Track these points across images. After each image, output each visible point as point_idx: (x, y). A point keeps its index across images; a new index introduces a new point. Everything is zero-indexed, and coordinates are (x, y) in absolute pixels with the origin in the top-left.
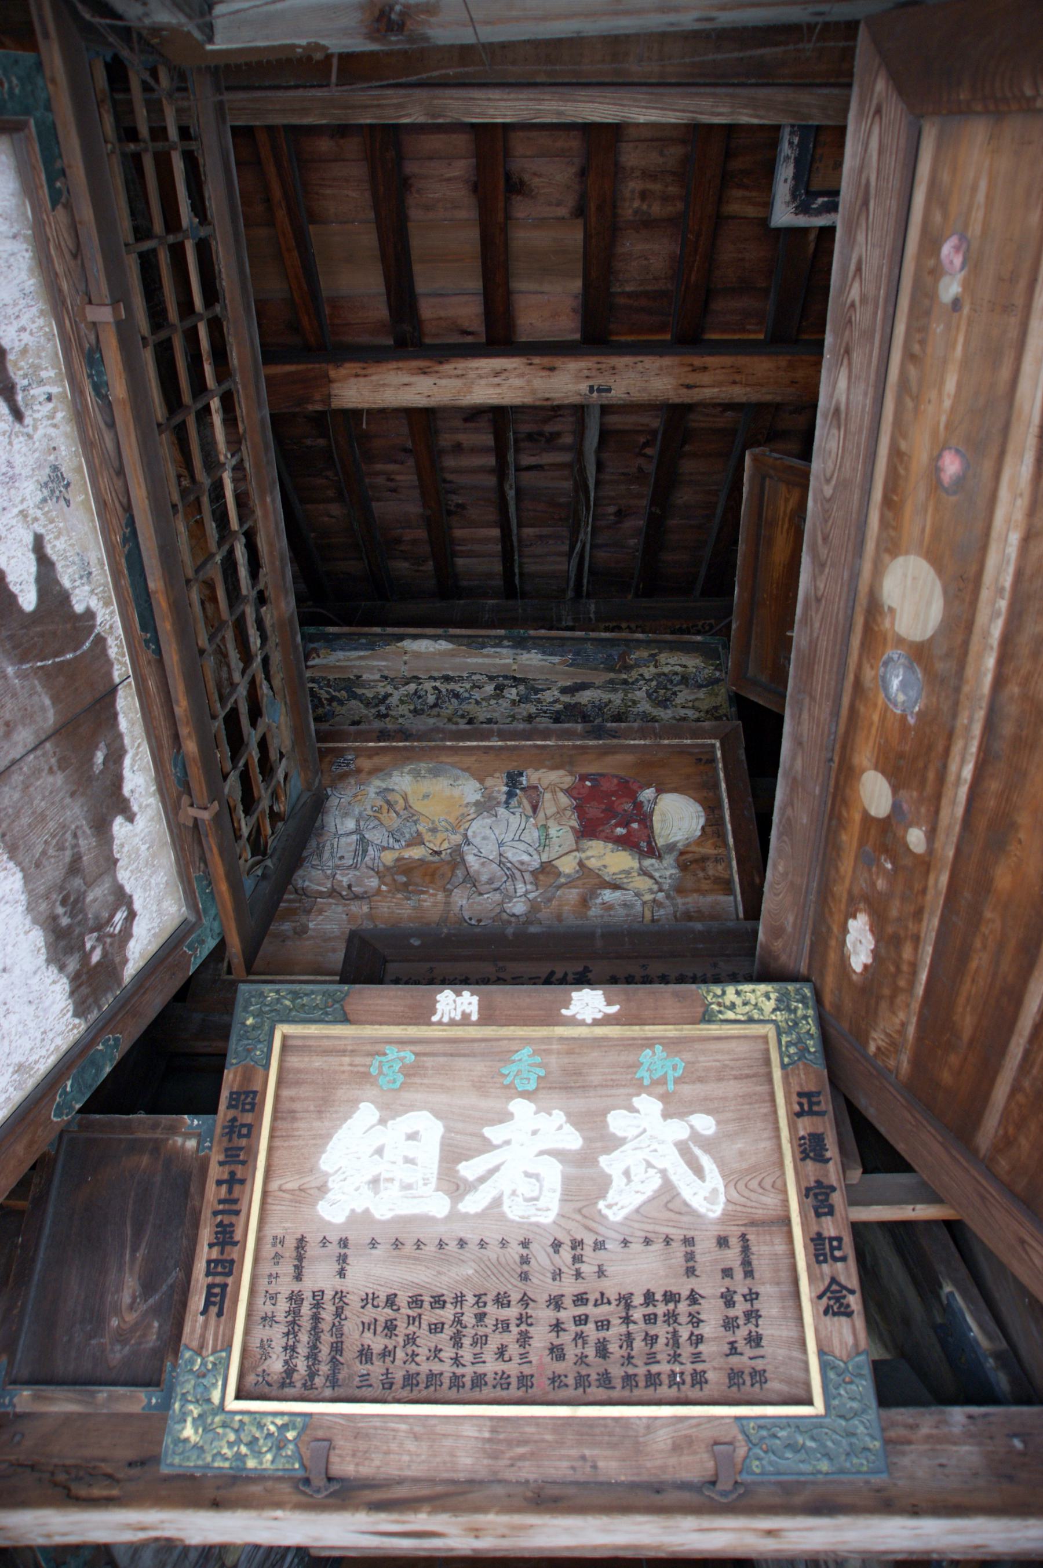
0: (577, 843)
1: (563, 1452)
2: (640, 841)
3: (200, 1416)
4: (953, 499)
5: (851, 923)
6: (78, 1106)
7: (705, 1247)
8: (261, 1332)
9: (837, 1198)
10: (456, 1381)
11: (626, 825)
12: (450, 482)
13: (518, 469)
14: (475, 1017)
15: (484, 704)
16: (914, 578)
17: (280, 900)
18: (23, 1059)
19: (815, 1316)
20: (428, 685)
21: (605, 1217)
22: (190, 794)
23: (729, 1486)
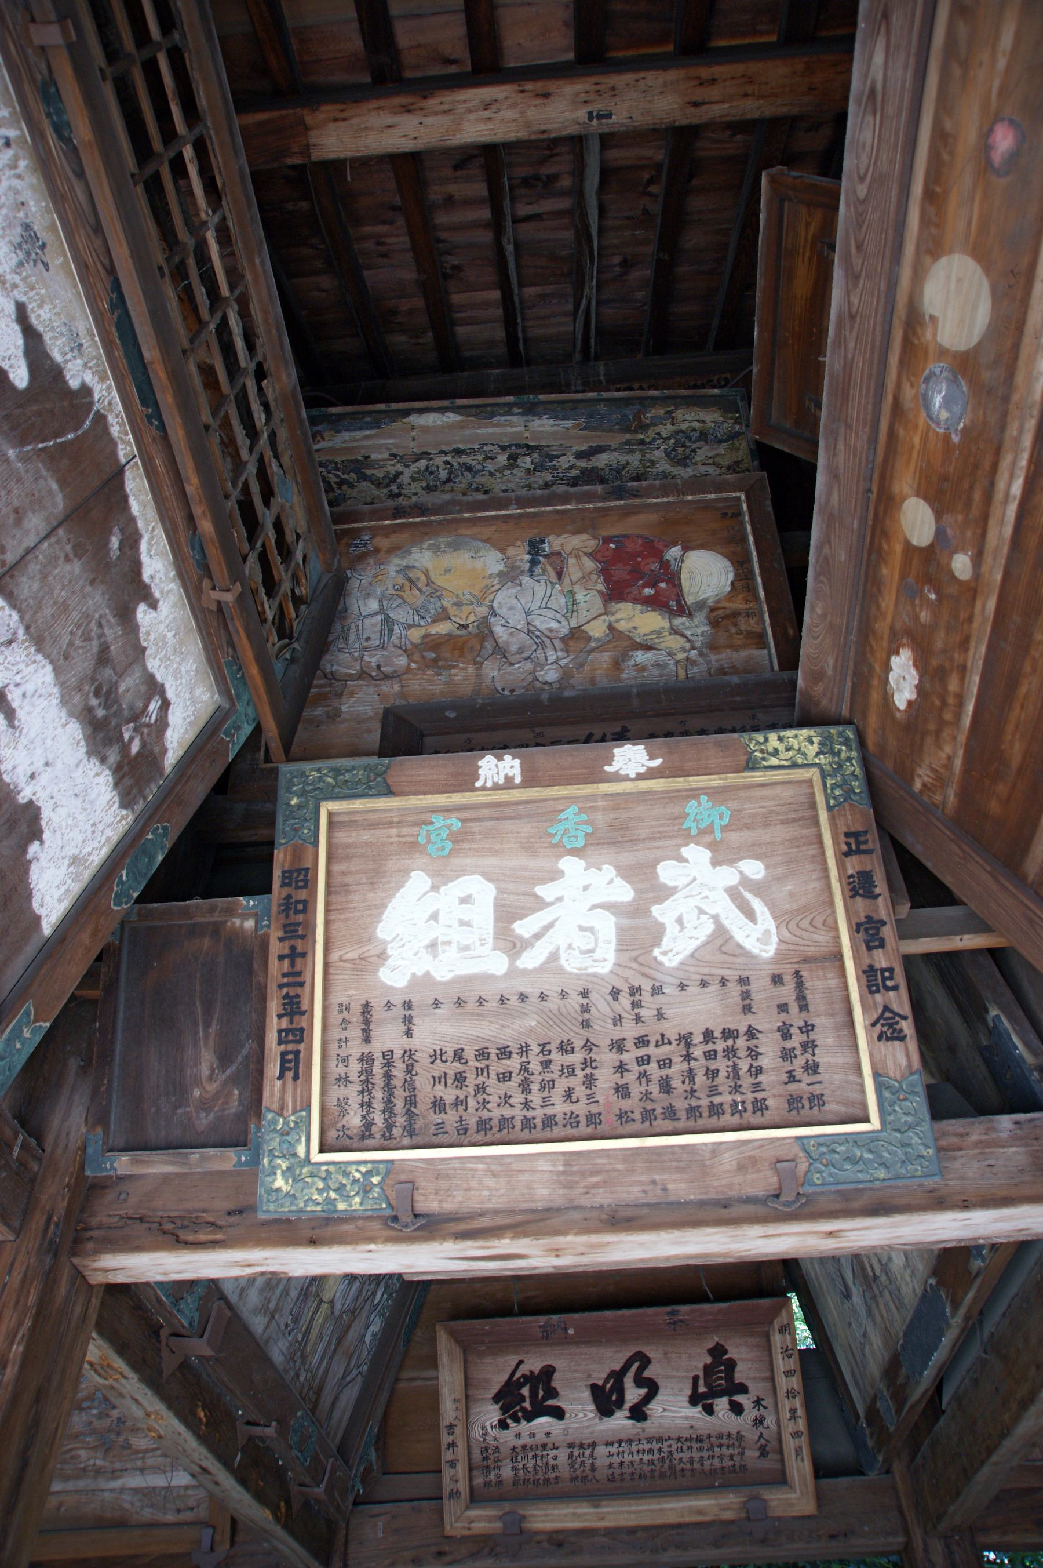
0: (605, 606)
1: (634, 1178)
2: (670, 601)
3: (288, 1168)
4: (1003, 181)
5: (895, 661)
6: (136, 895)
7: (760, 988)
8: (336, 1093)
9: (888, 932)
10: (528, 1123)
11: (654, 585)
12: (443, 241)
13: (516, 221)
14: (518, 780)
15: (498, 475)
16: (959, 280)
17: (310, 686)
18: (77, 852)
19: (869, 1042)
20: (439, 461)
21: (661, 964)
22: (211, 578)
23: (791, 1198)
